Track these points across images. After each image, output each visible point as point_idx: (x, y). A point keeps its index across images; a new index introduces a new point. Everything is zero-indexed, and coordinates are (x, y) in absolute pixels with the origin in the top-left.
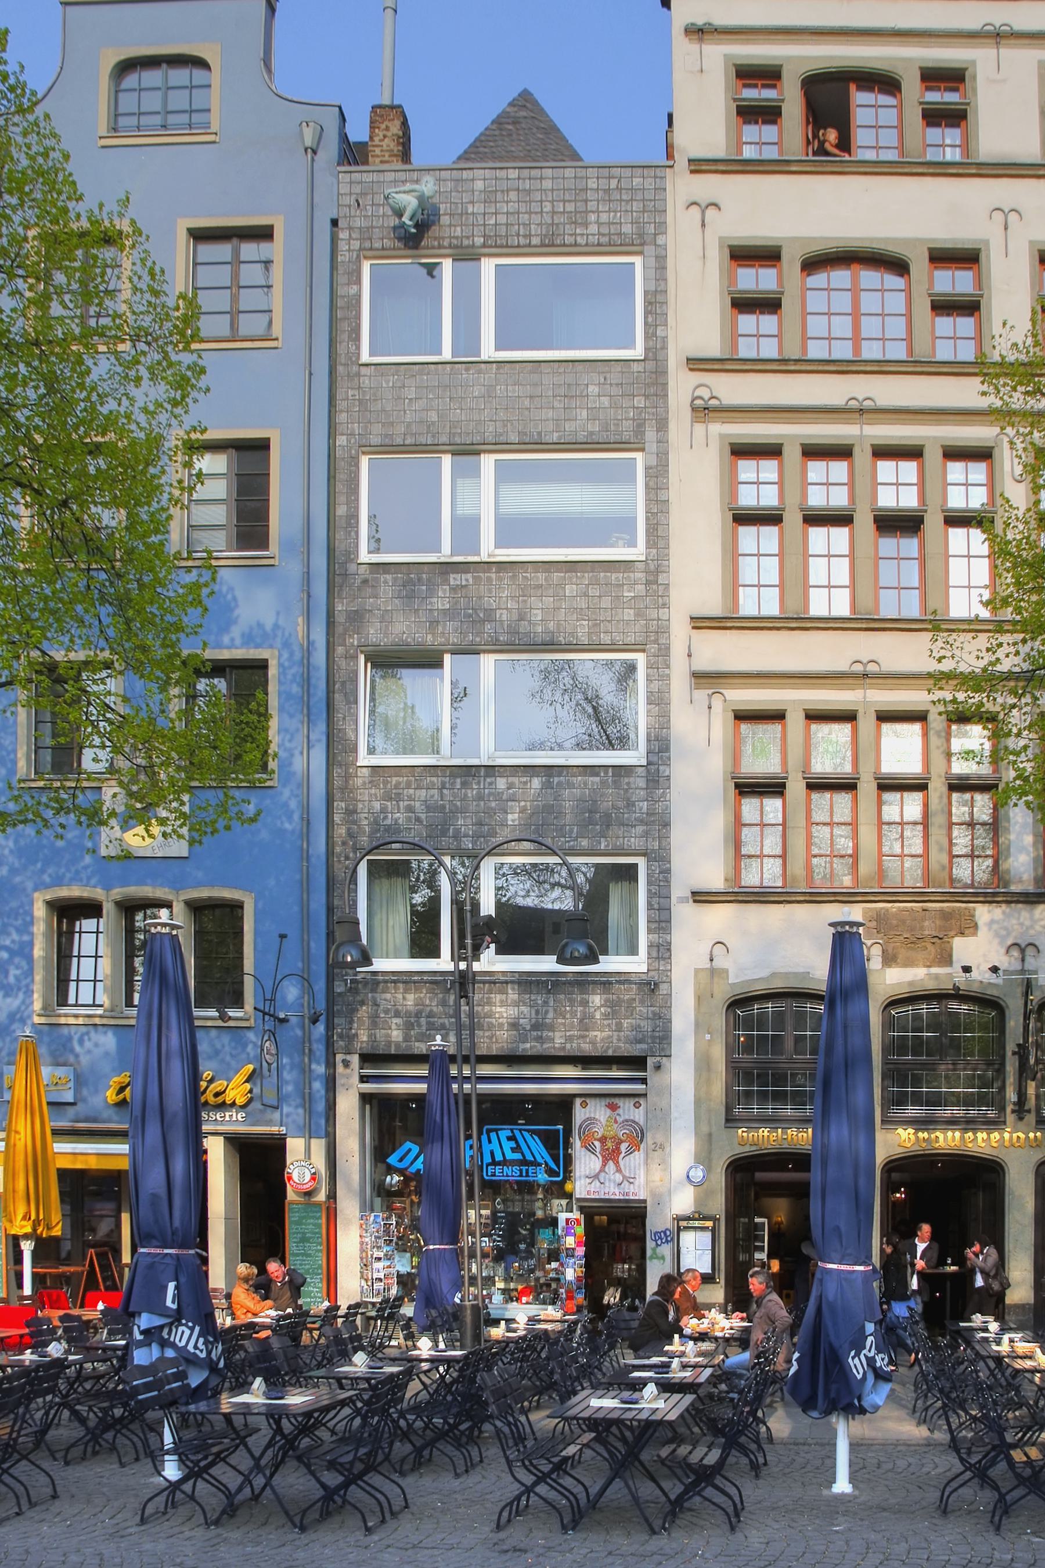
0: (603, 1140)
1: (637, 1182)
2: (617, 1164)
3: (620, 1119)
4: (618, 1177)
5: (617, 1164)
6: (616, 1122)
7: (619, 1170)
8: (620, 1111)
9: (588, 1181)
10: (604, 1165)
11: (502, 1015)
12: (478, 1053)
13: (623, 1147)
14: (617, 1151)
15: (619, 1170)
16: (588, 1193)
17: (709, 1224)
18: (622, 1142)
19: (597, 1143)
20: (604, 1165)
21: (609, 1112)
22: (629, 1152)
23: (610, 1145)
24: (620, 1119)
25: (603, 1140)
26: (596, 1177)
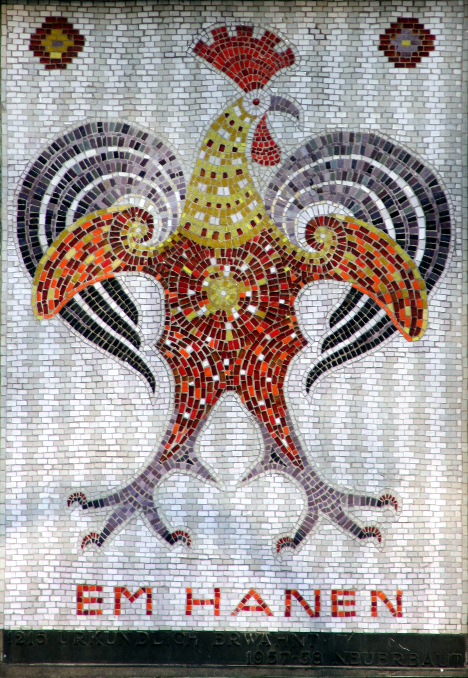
0: (180, 266)
1: (399, 530)
2: (271, 411)
3: (290, 136)
4: (281, 499)
5: (271, 411)
6: (265, 148)
7: (284, 452)
8: (292, 83)
9: (84, 522)
10: (189, 418)
11: (459, 219)
12: (397, 332)
13: (315, 307)
14: (273, 328)
15: (284, 452)
16: (85, 596)
17: (86, 607)
18: (305, 274)
19: (143, 290)
20: (189, 418)
21: (218, 88)
22: (351, 339)
23: (224, 292)
24: (290, 136)
25: (180, 266)
26: (136, 499)
